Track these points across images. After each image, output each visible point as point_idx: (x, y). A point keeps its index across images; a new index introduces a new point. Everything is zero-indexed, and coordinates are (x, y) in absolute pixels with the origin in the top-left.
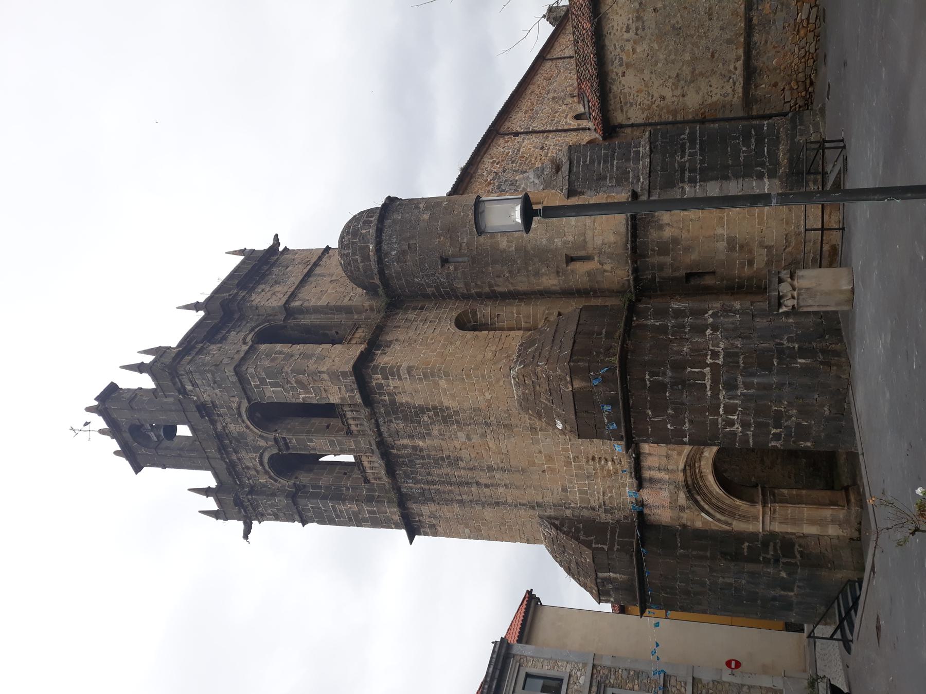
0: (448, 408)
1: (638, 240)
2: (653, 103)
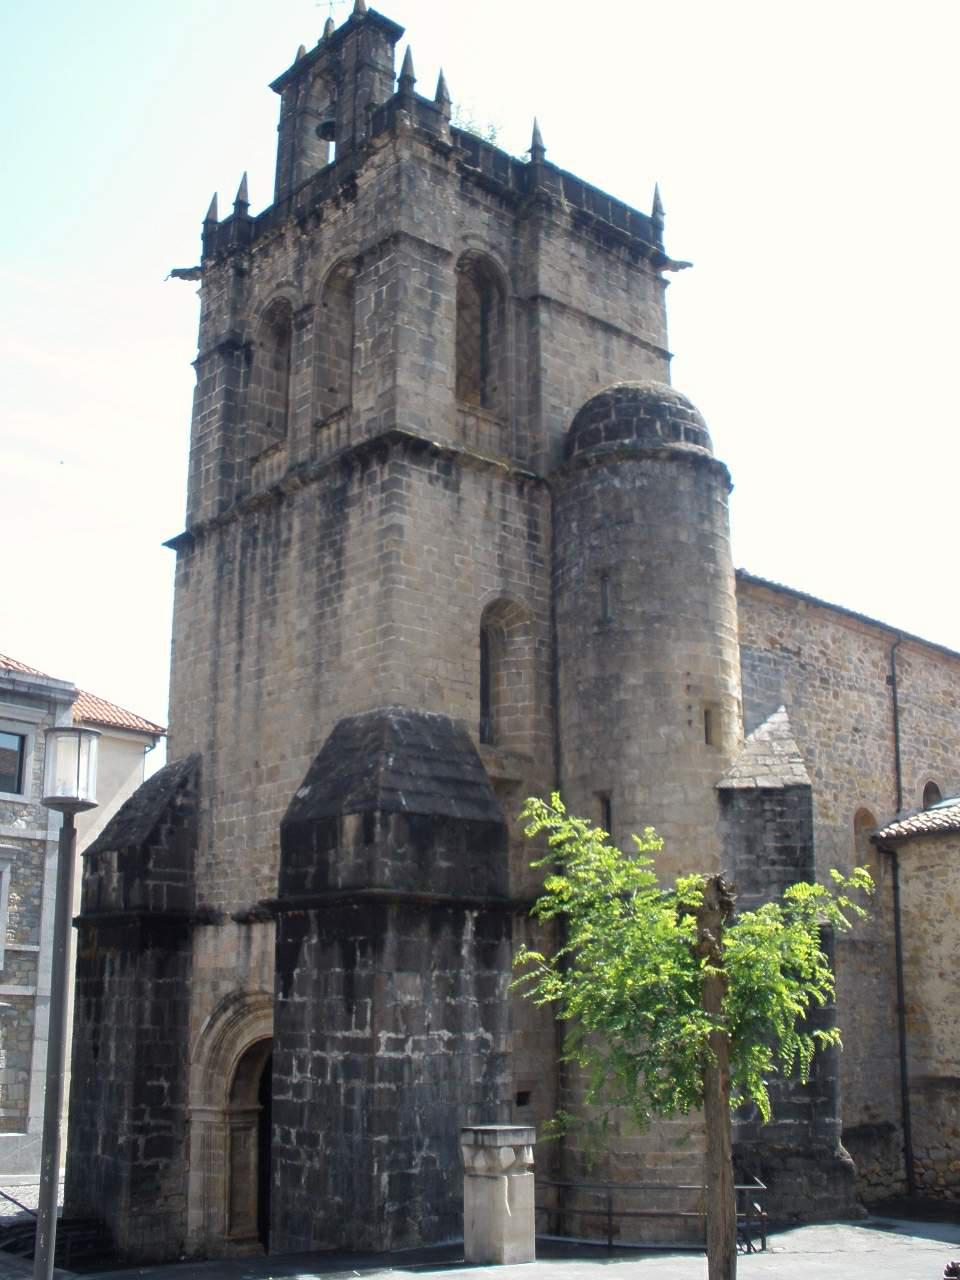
0: (340, 598)
2: (931, 922)
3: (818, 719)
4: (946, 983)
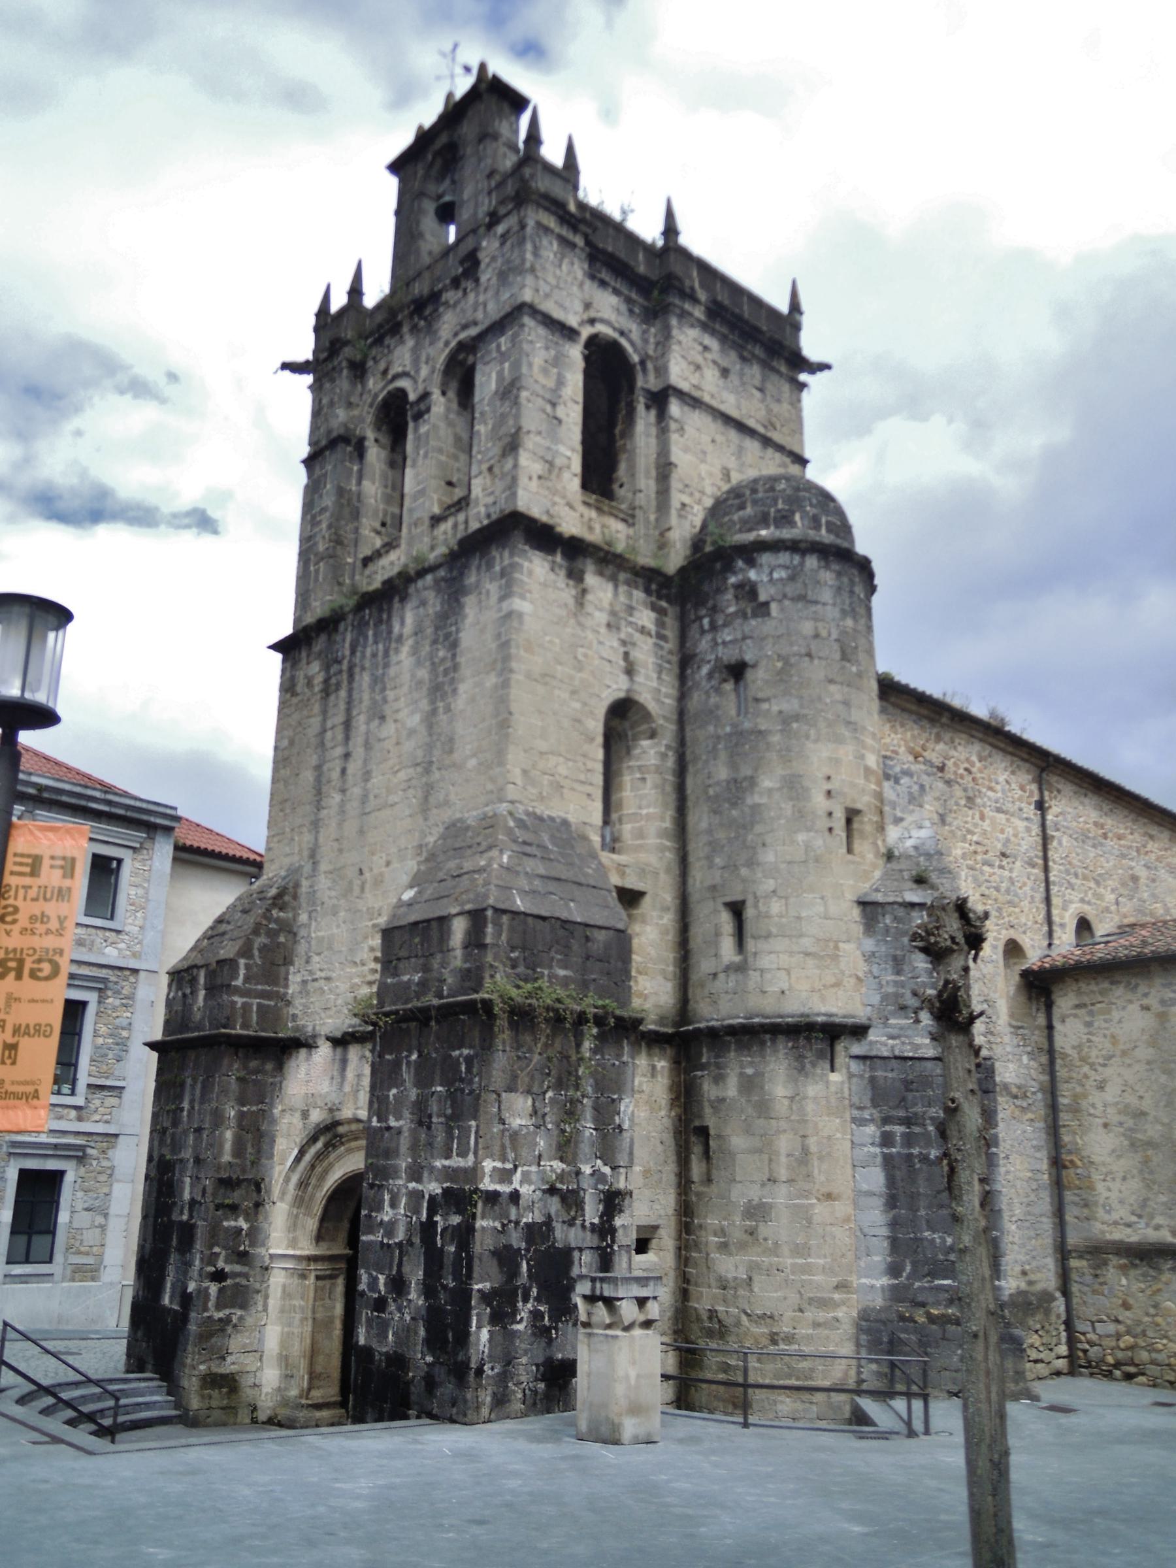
0: (455, 691)
3: (964, 840)
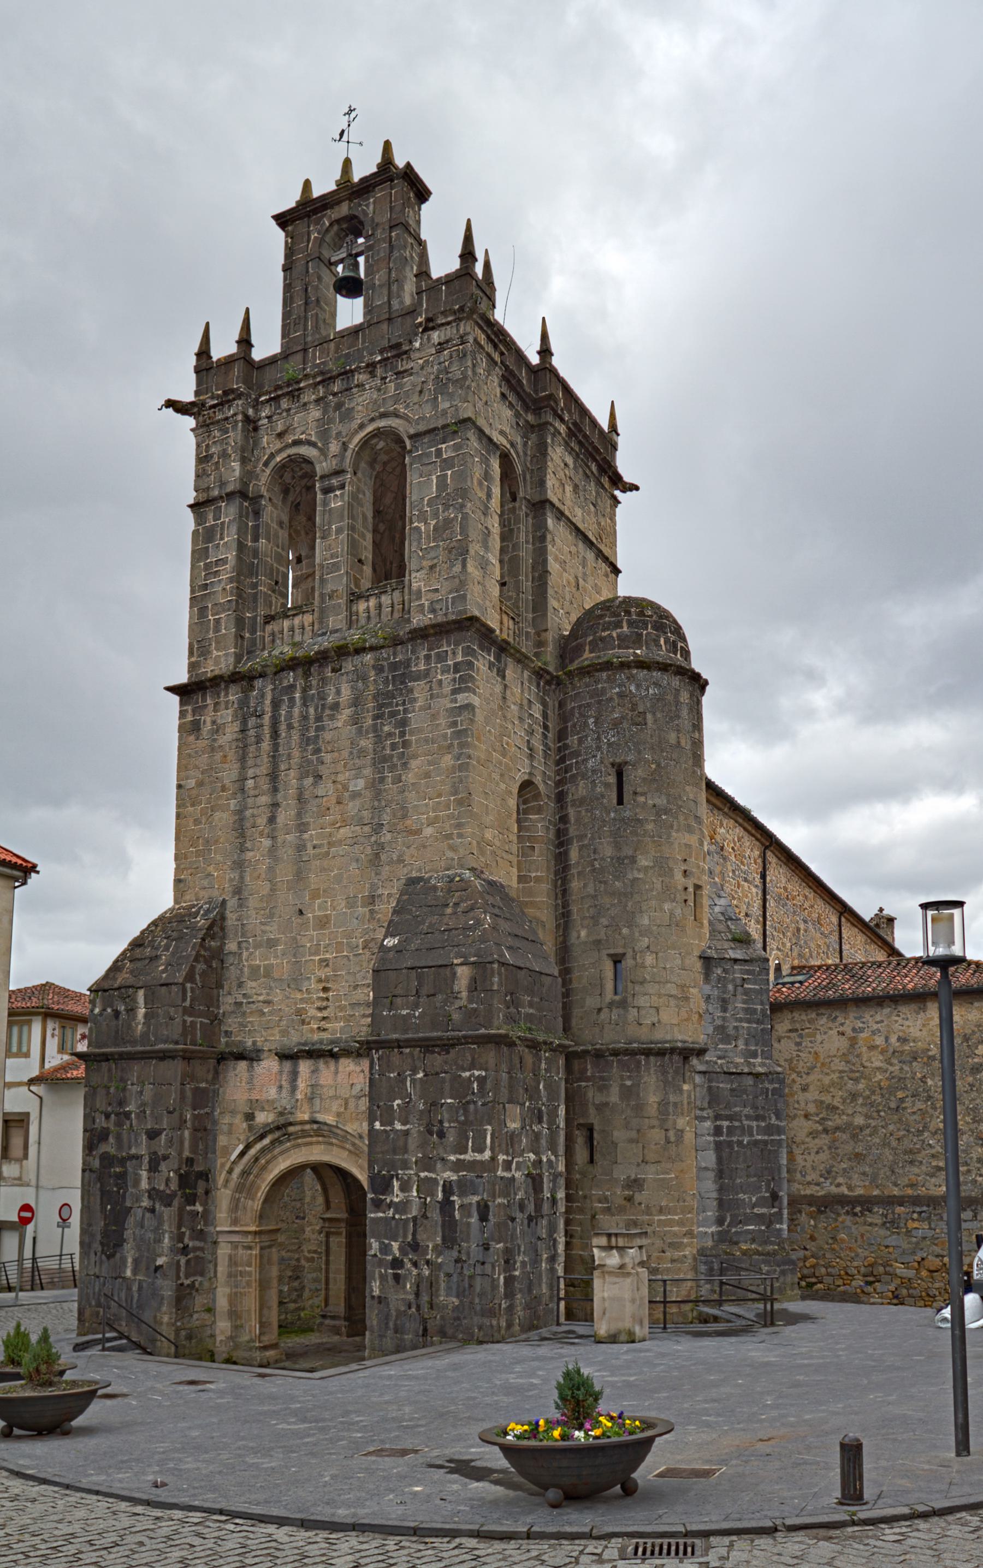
0: (405, 765)
1: (643, 1057)
2: (799, 1073)
4: (810, 1122)
